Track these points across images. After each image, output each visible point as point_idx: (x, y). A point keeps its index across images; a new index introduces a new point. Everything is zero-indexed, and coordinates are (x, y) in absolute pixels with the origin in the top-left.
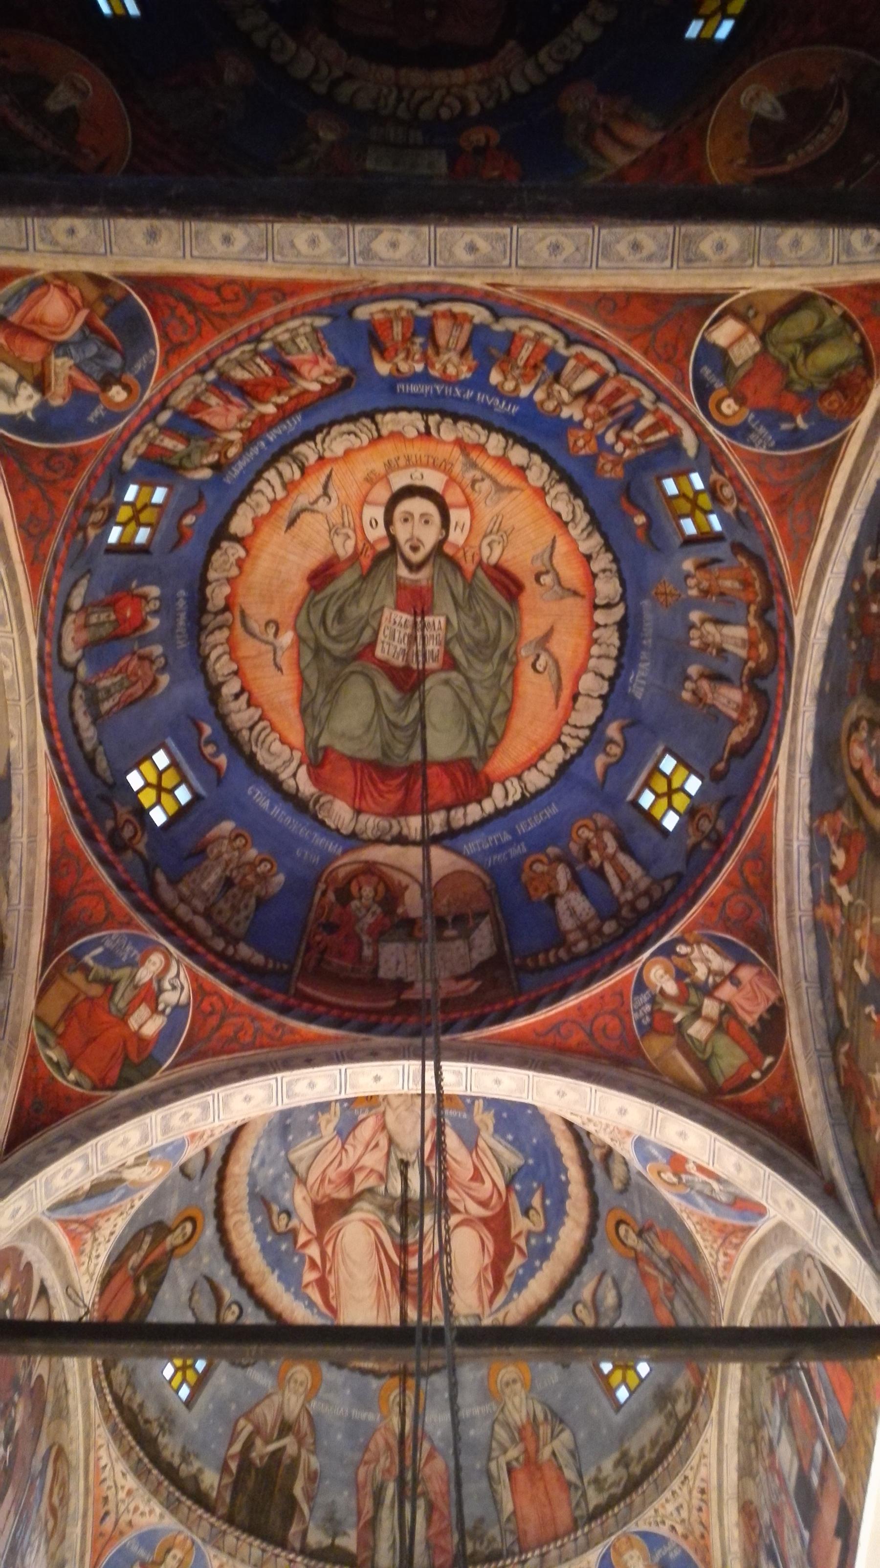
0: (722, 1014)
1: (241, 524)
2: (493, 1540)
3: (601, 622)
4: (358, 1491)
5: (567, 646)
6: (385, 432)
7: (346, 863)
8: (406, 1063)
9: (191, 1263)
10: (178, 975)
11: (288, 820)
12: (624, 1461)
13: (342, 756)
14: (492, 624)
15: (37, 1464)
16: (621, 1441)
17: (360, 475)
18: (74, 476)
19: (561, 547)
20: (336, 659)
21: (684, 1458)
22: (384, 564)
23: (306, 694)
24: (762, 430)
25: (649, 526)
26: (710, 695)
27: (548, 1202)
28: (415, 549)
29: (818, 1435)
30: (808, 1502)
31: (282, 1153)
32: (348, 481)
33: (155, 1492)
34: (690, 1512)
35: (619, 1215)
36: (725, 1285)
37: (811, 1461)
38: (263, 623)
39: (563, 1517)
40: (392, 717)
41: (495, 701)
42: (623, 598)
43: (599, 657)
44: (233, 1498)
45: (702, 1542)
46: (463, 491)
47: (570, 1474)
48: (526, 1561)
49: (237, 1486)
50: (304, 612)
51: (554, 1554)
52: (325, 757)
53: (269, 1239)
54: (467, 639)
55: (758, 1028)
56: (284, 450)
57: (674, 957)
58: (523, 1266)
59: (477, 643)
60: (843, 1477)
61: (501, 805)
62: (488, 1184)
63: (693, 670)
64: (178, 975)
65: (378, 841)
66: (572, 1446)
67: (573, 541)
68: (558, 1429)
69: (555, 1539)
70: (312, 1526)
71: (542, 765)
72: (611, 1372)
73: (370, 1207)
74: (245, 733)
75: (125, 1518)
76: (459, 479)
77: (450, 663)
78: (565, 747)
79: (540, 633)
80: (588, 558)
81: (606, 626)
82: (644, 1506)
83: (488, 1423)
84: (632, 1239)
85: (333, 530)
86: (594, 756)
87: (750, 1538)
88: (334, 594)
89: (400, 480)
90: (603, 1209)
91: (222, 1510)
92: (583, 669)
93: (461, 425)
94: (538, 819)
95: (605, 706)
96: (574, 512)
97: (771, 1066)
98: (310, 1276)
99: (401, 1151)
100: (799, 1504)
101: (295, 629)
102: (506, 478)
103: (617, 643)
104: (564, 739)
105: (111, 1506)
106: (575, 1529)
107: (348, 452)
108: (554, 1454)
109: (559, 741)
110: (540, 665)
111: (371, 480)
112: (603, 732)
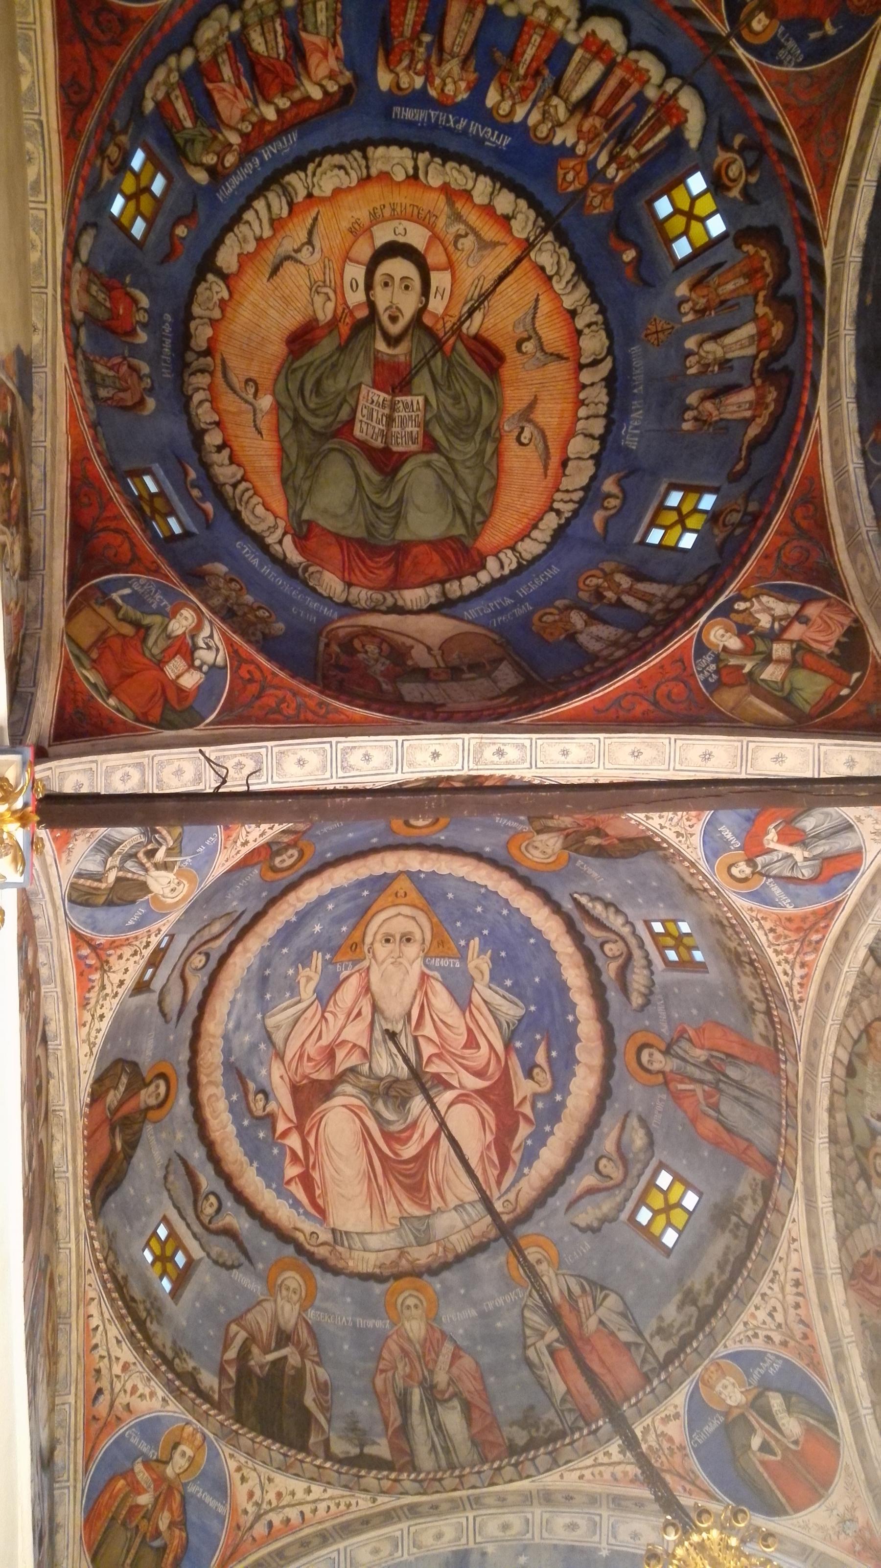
0: (794, 652)
1: (227, 258)
3: (587, 382)
4: (379, 1401)
5: (551, 414)
6: (374, 172)
7: (344, 625)
8: (466, 736)
9: (164, 1135)
10: (211, 636)
11: (280, 581)
12: (690, 1298)
13: (326, 532)
14: (473, 402)
16: (680, 1281)
17: (345, 225)
18: (120, 45)
19: (545, 306)
20: (314, 432)
22: (362, 336)
23: (286, 465)
24: (791, 44)
25: (639, 259)
26: (715, 413)
27: (554, 1054)
28: (394, 319)
31: (259, 1016)
32: (334, 225)
35: (640, 1039)
36: (801, 1012)
38: (243, 380)
40: (374, 498)
41: (480, 480)
42: (610, 351)
43: (587, 418)
46: (446, 250)
48: (598, 1429)
49: (240, 1390)
50: (282, 376)
52: (309, 530)
53: (246, 1123)
54: (447, 420)
55: (837, 652)
56: (274, 179)
57: (733, 615)
58: (530, 1136)
59: (457, 422)
61: (497, 575)
62: (484, 1048)
63: (692, 399)
64: (211, 636)
65: (374, 610)
66: (621, 1308)
67: (558, 296)
68: (600, 1297)
71: (535, 534)
72: (651, 1222)
73: (354, 1091)
74: (229, 489)
75: (123, 1399)
76: (442, 235)
77: (431, 445)
78: (558, 512)
79: (523, 405)
80: (573, 313)
81: (592, 384)
82: (730, 1324)
83: (516, 1311)
84: (658, 1061)
85: (315, 288)
86: (593, 513)
88: (312, 363)
89: (383, 235)
90: (619, 1040)
92: (571, 434)
93: (450, 165)
94: (540, 581)
95: (598, 465)
96: (558, 263)
97: (859, 681)
98: (292, 1171)
99: (385, 1019)
101: (274, 394)
102: (490, 232)
103: (605, 399)
104: (556, 505)
105: (105, 1383)
106: (648, 1380)
107: (337, 191)
108: (601, 1322)
109: (551, 509)
110: (525, 437)
111: (357, 231)
112: (599, 489)
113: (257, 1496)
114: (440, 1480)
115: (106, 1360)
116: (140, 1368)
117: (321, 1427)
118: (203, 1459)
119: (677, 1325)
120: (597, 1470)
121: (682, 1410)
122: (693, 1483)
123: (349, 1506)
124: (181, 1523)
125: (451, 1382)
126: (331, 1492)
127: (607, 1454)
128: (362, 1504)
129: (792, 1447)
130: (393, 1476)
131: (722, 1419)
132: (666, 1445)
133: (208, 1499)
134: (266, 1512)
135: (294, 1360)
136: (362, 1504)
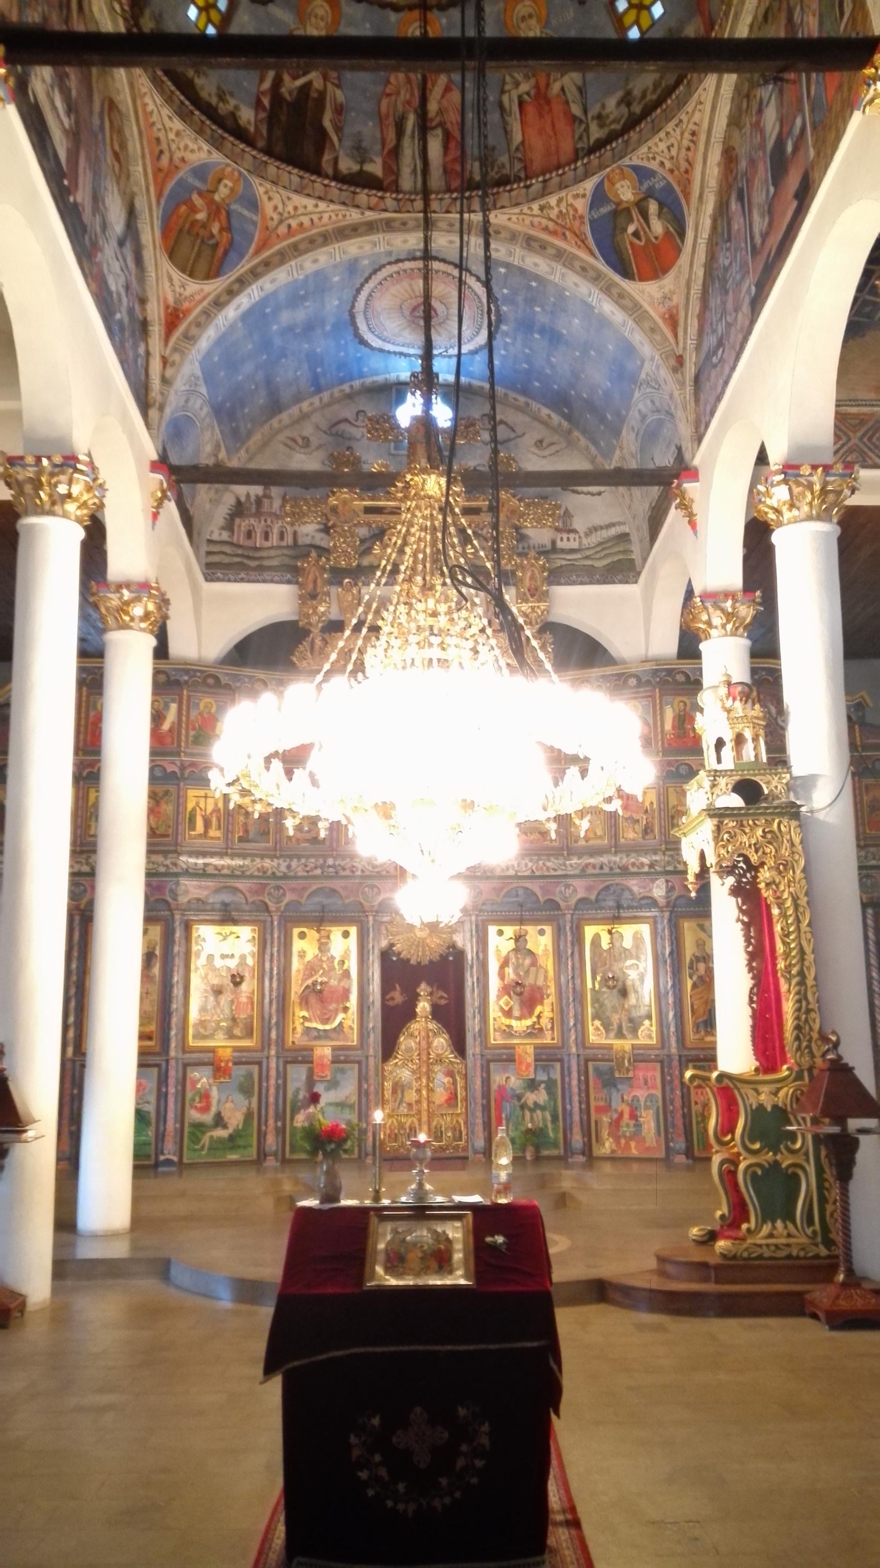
2: (503, 166)
12: (626, 100)
15: (96, 121)
21: (682, 103)
29: (801, 110)
30: (779, 164)
33: (200, 132)
34: (679, 149)
37: (790, 133)
39: (567, 147)
44: (270, 131)
45: (686, 176)
47: (576, 110)
48: (531, 185)
49: (272, 119)
51: (556, 180)
60: (812, 152)
69: (558, 168)
70: (341, 154)
82: (640, 143)
87: (727, 179)
91: (261, 144)
100: (771, 161)
105: (164, 146)
106: (576, 160)
108: (563, 89)
113: (280, 209)
114: (412, 201)
115: (163, 131)
116: (189, 132)
117: (333, 145)
118: (241, 188)
119: (612, 117)
120: (521, 217)
121: (589, 193)
122: (583, 242)
123: (344, 216)
124: (227, 228)
125: (440, 112)
126: (332, 207)
127: (530, 209)
128: (354, 216)
129: (653, 240)
130: (380, 194)
131: (614, 207)
132: (571, 212)
133: (246, 213)
134: (287, 219)
135: (318, 84)
136: (354, 216)
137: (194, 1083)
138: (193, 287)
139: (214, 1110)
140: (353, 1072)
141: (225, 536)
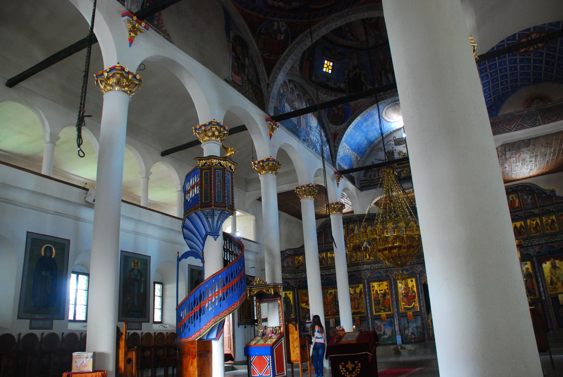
137: (377, 324)
138: (338, 127)
139: (383, 331)
140: (419, 318)
141: (364, 178)
